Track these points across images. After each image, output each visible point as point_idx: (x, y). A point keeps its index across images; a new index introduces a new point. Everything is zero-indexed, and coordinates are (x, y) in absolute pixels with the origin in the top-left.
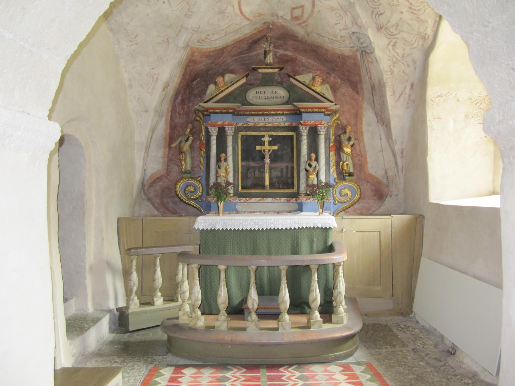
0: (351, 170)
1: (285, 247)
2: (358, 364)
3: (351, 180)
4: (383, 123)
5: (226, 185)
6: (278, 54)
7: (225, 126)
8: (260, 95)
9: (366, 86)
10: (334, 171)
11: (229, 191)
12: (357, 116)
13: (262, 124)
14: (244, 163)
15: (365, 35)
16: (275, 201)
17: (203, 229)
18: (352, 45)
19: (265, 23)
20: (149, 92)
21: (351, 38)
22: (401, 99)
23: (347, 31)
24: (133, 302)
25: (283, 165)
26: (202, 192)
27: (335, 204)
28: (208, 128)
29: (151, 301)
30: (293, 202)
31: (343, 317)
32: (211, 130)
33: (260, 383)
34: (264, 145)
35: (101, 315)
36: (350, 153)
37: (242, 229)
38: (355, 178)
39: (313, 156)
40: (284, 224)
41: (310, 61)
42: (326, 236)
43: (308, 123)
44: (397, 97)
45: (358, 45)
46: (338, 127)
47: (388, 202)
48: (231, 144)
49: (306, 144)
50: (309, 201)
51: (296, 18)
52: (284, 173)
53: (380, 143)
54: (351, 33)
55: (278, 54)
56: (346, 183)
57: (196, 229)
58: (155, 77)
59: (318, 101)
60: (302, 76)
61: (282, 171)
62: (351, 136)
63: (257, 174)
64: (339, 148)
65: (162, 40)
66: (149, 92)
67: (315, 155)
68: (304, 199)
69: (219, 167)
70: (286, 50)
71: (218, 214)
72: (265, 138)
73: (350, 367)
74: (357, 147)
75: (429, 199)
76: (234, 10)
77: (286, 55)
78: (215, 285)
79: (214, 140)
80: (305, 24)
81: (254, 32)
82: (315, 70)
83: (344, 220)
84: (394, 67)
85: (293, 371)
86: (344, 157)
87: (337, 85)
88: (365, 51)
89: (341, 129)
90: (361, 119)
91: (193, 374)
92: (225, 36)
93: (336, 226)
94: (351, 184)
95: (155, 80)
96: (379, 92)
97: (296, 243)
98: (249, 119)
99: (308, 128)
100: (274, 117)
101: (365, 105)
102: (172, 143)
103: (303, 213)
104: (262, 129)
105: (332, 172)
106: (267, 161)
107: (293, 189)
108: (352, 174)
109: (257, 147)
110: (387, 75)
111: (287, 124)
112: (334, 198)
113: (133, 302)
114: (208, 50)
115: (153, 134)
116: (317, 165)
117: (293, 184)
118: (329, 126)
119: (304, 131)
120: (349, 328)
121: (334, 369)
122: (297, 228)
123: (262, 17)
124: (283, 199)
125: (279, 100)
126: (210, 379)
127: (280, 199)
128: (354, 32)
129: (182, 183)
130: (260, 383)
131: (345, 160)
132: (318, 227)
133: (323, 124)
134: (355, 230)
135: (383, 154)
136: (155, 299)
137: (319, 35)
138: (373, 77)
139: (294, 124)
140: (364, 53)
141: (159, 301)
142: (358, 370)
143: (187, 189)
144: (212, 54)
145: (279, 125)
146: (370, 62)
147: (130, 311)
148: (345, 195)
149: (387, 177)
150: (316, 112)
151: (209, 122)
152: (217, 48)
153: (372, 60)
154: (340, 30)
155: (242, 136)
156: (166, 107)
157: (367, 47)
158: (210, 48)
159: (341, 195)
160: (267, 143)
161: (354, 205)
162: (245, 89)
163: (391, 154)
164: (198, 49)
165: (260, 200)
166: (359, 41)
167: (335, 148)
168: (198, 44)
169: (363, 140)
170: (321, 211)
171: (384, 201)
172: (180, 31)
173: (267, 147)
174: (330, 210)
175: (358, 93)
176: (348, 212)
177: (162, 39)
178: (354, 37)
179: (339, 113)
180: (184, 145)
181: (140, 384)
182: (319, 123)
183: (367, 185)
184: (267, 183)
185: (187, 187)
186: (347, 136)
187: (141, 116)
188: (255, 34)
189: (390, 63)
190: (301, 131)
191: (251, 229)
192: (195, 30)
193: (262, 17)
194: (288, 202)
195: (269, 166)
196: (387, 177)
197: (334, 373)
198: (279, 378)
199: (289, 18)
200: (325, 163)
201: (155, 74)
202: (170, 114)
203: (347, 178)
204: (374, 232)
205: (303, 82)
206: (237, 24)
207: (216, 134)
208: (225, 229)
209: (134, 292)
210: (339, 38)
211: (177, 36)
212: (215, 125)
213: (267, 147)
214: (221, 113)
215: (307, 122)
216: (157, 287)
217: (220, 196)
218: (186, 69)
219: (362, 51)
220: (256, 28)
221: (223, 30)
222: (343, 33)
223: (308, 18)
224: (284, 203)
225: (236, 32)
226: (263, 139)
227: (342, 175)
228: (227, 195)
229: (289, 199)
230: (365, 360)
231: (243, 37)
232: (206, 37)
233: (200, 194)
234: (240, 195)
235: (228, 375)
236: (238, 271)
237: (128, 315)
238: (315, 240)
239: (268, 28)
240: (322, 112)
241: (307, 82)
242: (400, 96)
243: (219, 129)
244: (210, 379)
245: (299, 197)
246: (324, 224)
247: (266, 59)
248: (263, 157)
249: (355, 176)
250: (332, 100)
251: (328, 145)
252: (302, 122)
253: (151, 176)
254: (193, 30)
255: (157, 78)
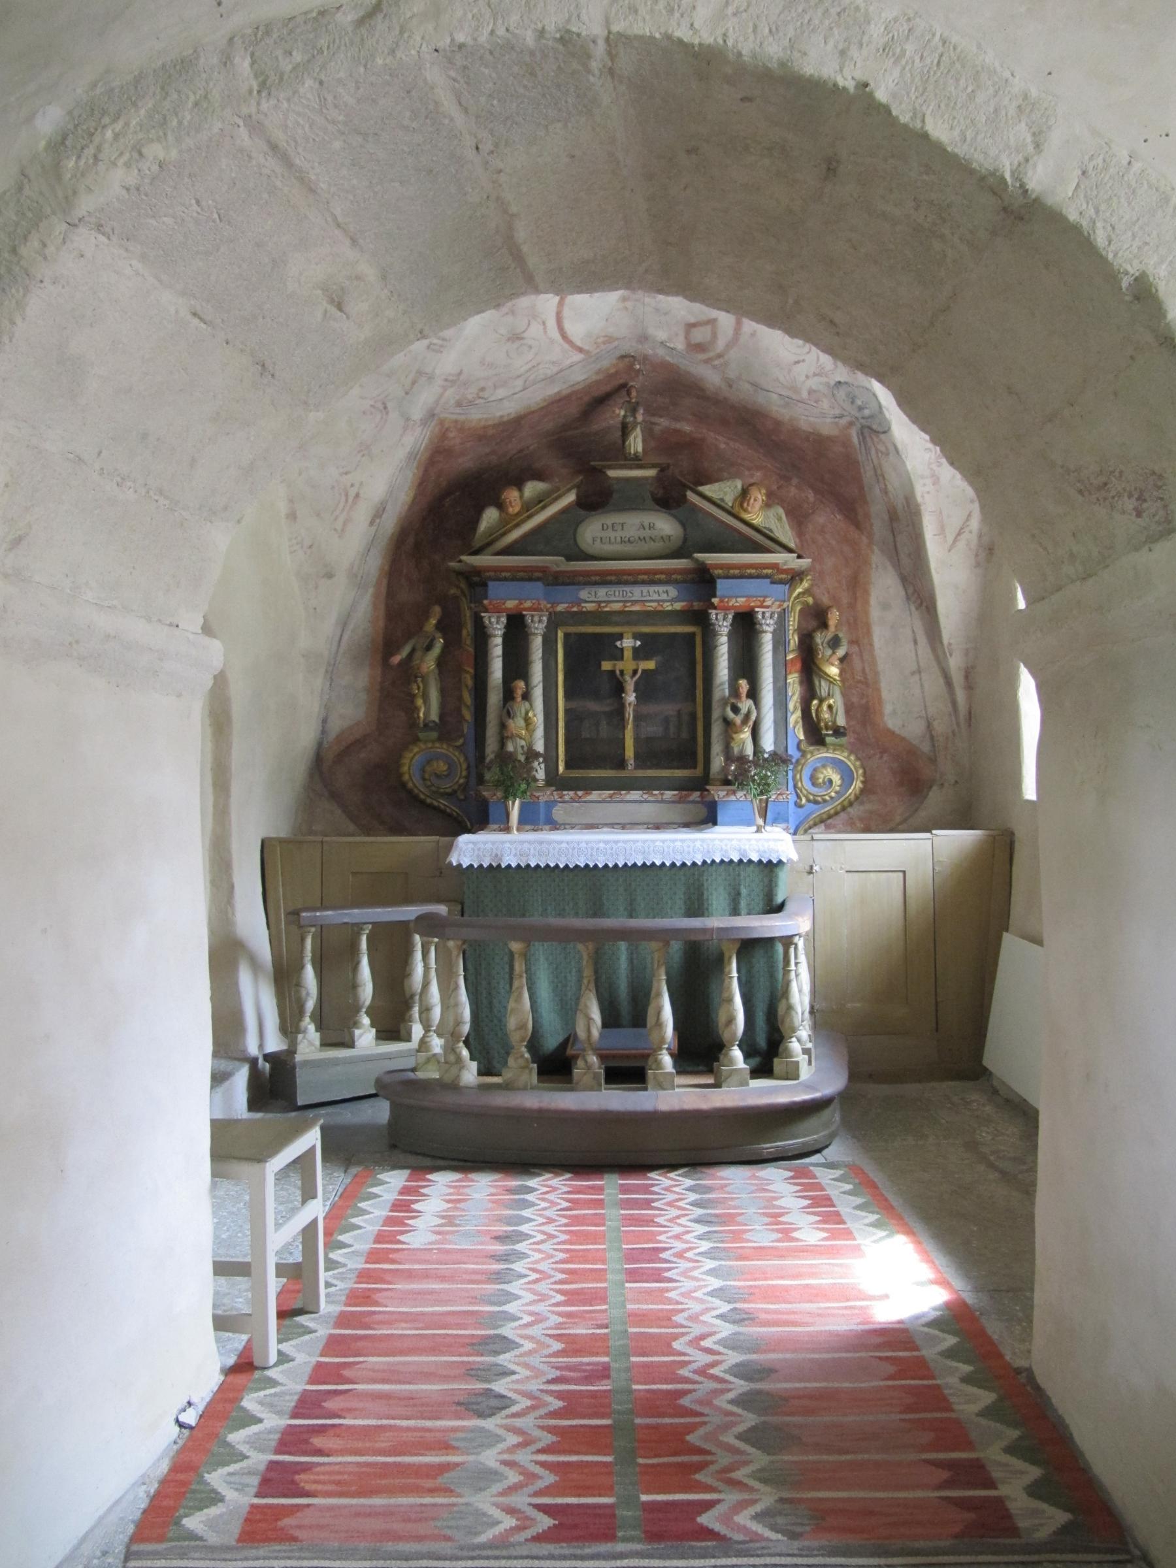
0: (841, 721)
1: (671, 908)
2: (831, 1166)
3: (841, 746)
4: (919, 601)
5: (527, 759)
6: (657, 429)
7: (524, 613)
8: (612, 535)
9: (877, 509)
10: (796, 723)
11: (534, 773)
12: (857, 585)
13: (616, 607)
14: (574, 704)
15: (867, 389)
16: (651, 799)
17: (471, 866)
18: (837, 412)
19: (622, 357)
20: (335, 530)
21: (833, 395)
22: (961, 544)
23: (824, 380)
24: (304, 1038)
25: (669, 709)
26: (467, 777)
27: (801, 806)
28: (482, 618)
29: (347, 1039)
30: (693, 802)
31: (797, 1063)
32: (490, 621)
33: (602, 1197)
34: (622, 659)
35: (231, 1067)
36: (838, 678)
37: (567, 866)
38: (852, 740)
39: (744, 685)
40: (668, 853)
41: (737, 445)
42: (771, 881)
43: (730, 604)
44: (950, 539)
45: (852, 413)
46: (807, 612)
47: (935, 799)
48: (541, 655)
49: (726, 657)
50: (733, 798)
51: (700, 348)
52: (672, 729)
53: (913, 651)
54: (832, 383)
55: (657, 429)
56: (827, 752)
57: (455, 864)
58: (352, 492)
59: (758, 549)
60: (716, 486)
61: (666, 721)
62: (841, 635)
63: (605, 730)
64: (809, 666)
65: (372, 406)
66: (335, 530)
67: (749, 683)
68: (722, 794)
69: (509, 713)
70: (677, 419)
71: (507, 829)
72: (625, 640)
73: (811, 1171)
74: (857, 663)
75: (1024, 790)
76: (545, 332)
77: (677, 431)
78: (500, 1002)
79: (497, 646)
80: (721, 360)
81: (595, 378)
82: (749, 469)
83: (815, 843)
84: (939, 466)
85: (678, 1178)
86: (823, 688)
87: (806, 506)
88: (870, 428)
89: (817, 616)
90: (866, 592)
91: (453, 1182)
92: (524, 390)
93: (795, 856)
94: (840, 756)
95: (350, 500)
96: (908, 526)
97: (698, 900)
98: (584, 594)
99: (730, 616)
100: (645, 589)
101: (877, 558)
102: (392, 654)
103: (717, 828)
104: (615, 618)
105: (791, 725)
106: (631, 698)
107: (695, 767)
108: (842, 730)
109: (603, 663)
110: (925, 485)
111: (678, 606)
112: (796, 792)
113: (304, 1038)
114: (483, 423)
115: (343, 630)
116: (754, 707)
117: (694, 754)
118: (784, 610)
119: (723, 627)
120: (808, 1087)
121: (775, 1177)
122: (700, 864)
123: (616, 343)
124: (669, 794)
125: (657, 546)
126: (493, 1190)
127: (662, 794)
128: (840, 382)
129: (418, 753)
130: (602, 1197)
131: (824, 694)
132: (750, 861)
133: (767, 607)
134: (841, 869)
135: (920, 679)
136: (357, 1032)
137: (754, 385)
138: (889, 487)
139: (697, 605)
140: (866, 431)
141: (365, 1037)
142: (825, 1177)
143: (428, 769)
144: (491, 432)
145: (660, 609)
146: (882, 452)
147: (298, 1058)
148: (824, 783)
149: (932, 738)
150: (751, 577)
151: (486, 602)
152: (505, 419)
153: (886, 447)
154: (807, 377)
155: (567, 636)
156: (375, 564)
157: (871, 417)
158: (486, 420)
159: (814, 784)
160: (628, 654)
161: (850, 810)
162: (569, 521)
163: (941, 681)
164: (456, 421)
165: (611, 797)
166: (852, 403)
167: (798, 666)
168: (458, 410)
169: (871, 645)
170: (760, 822)
171: (925, 797)
172: (414, 383)
173: (627, 664)
174: (787, 821)
175: (858, 525)
176: (834, 827)
177: (372, 403)
178: (841, 394)
179: (809, 577)
180: (422, 660)
181: (336, 1198)
182: (759, 604)
183: (881, 757)
184: (630, 753)
185: (429, 762)
186: (830, 634)
187: (316, 588)
188: (597, 382)
189: (930, 458)
190: (714, 625)
191: (587, 866)
192: (451, 378)
193: (616, 343)
194: (680, 801)
195: (634, 710)
196: (932, 738)
197: (770, 1182)
198: (646, 1189)
199: (680, 345)
200: (775, 705)
201: (352, 485)
202: (385, 582)
203: (829, 740)
204: (890, 874)
205: (719, 502)
206: (553, 363)
207: (500, 633)
208: (523, 865)
209: (308, 1014)
210: (805, 395)
211: (407, 393)
212: (498, 610)
213: (627, 664)
214: (514, 579)
215: (727, 602)
216: (361, 1002)
217: (512, 785)
218: (426, 471)
219: (863, 427)
220: (600, 370)
221: (519, 376)
222: (813, 383)
223: (729, 346)
224: (673, 802)
225: (550, 379)
226: (618, 644)
227: (815, 734)
228: (528, 784)
229: (684, 793)
230: (848, 1159)
231: (569, 391)
232: (478, 394)
233: (462, 781)
234: (553, 780)
235: (533, 1182)
236: (557, 968)
237: (294, 1068)
238: (744, 891)
239: (630, 367)
240: (766, 577)
241: (729, 500)
242: (956, 538)
243: (510, 618)
244: (493, 1190)
245: (708, 787)
246: (765, 852)
247: (627, 443)
248: (619, 689)
249: (851, 734)
250: (792, 545)
251: (781, 657)
252: (715, 601)
253: (337, 737)
254: (446, 380)
255: (357, 495)
